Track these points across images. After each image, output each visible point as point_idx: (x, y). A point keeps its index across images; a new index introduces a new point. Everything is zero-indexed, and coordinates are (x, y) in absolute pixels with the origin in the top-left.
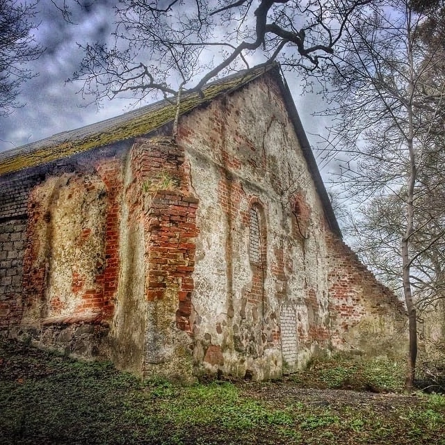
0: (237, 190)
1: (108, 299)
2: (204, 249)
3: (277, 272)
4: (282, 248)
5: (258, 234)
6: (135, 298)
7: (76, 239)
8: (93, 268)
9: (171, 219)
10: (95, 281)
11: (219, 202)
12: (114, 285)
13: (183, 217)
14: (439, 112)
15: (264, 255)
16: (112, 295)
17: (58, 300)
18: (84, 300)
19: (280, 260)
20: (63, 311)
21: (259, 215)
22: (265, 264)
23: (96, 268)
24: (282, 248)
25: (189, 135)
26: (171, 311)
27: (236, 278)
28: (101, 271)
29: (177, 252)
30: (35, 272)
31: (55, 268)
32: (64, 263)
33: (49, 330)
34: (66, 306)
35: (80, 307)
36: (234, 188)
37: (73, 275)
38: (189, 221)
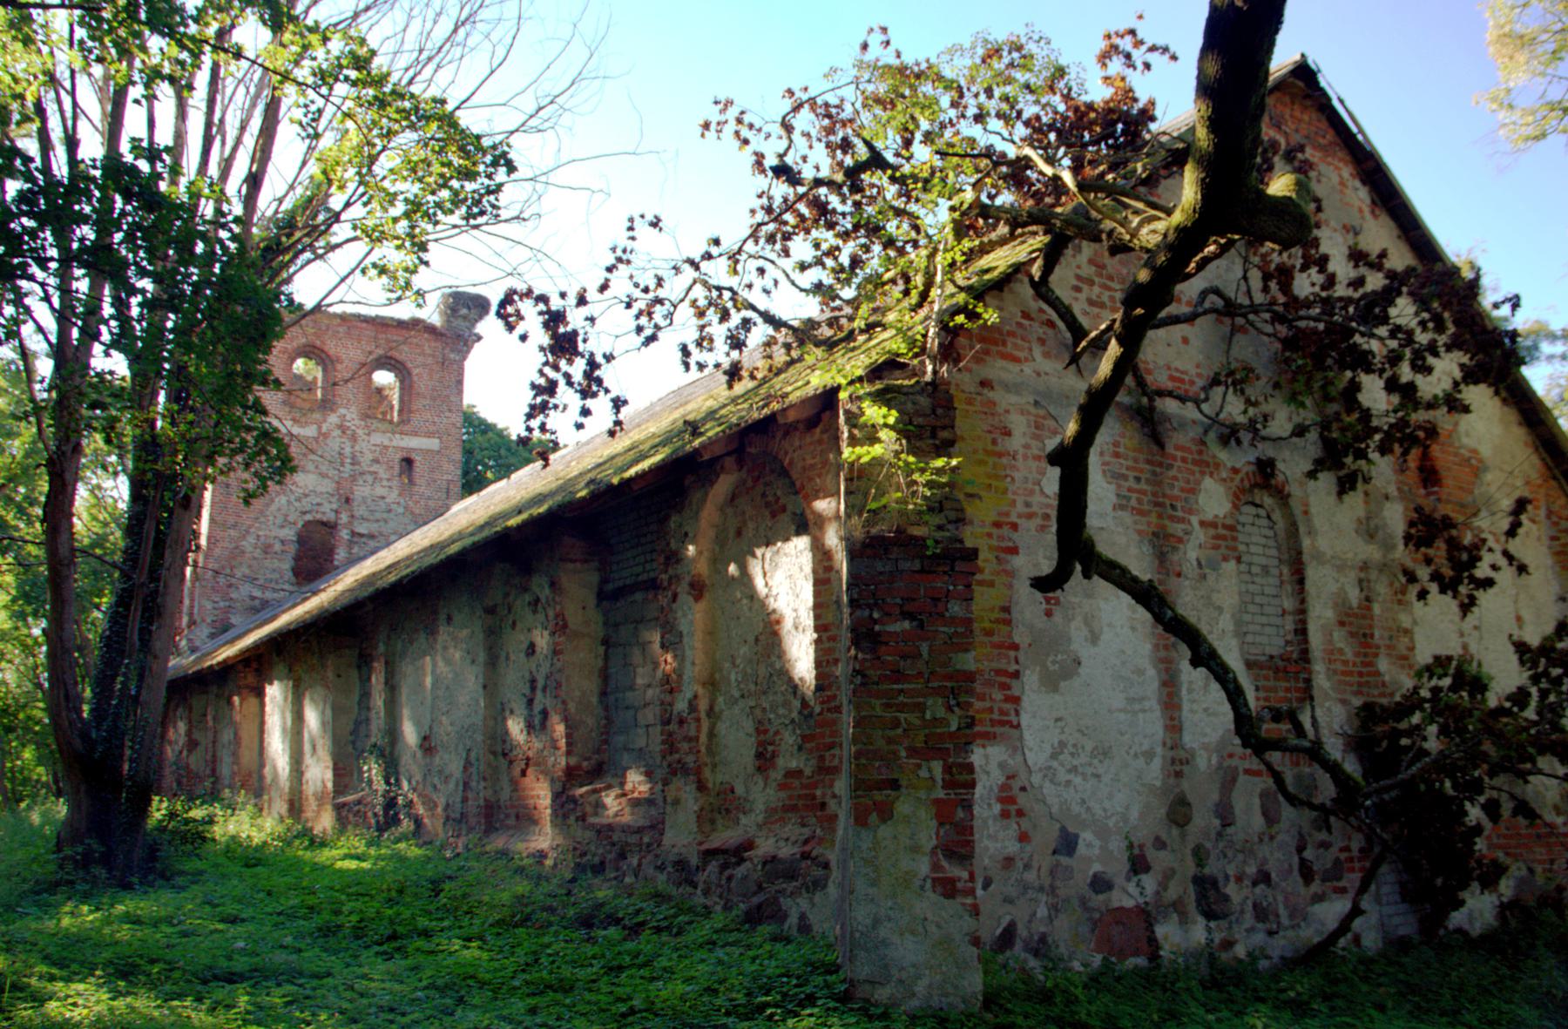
0: (1184, 460)
1: (824, 795)
2: (1074, 646)
3: (1350, 673)
4: (1368, 599)
5: (1275, 571)
6: (1510, 519)
7: (757, 640)
8: (795, 715)
9: (906, 608)
10: (800, 749)
11: (1122, 507)
12: (836, 762)
13: (939, 599)
14: (1363, 361)
15: (1302, 631)
16: (831, 786)
17: (732, 791)
18: (783, 794)
19: (1363, 639)
20: (744, 820)
21: (1277, 516)
22: (1305, 655)
23: (800, 713)
24: (1368, 599)
25: (1010, 340)
26: (915, 849)
27: (1192, 711)
28: (812, 722)
29: (924, 696)
30: (681, 722)
31: (721, 711)
32: (736, 702)
33: (713, 867)
34: (748, 806)
35: (775, 810)
36: (1174, 458)
37: (758, 731)
38: (955, 608)
